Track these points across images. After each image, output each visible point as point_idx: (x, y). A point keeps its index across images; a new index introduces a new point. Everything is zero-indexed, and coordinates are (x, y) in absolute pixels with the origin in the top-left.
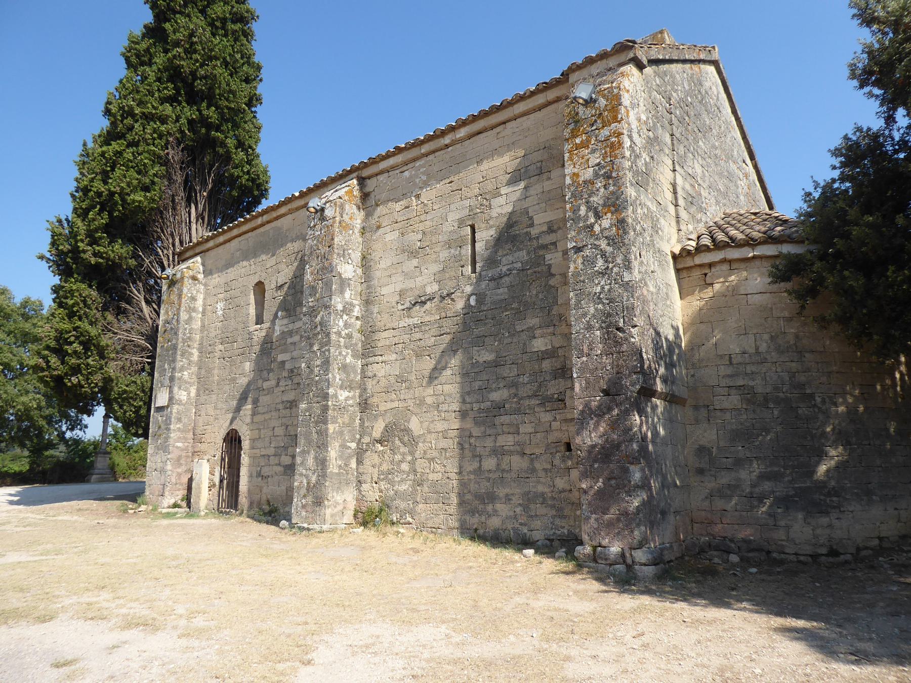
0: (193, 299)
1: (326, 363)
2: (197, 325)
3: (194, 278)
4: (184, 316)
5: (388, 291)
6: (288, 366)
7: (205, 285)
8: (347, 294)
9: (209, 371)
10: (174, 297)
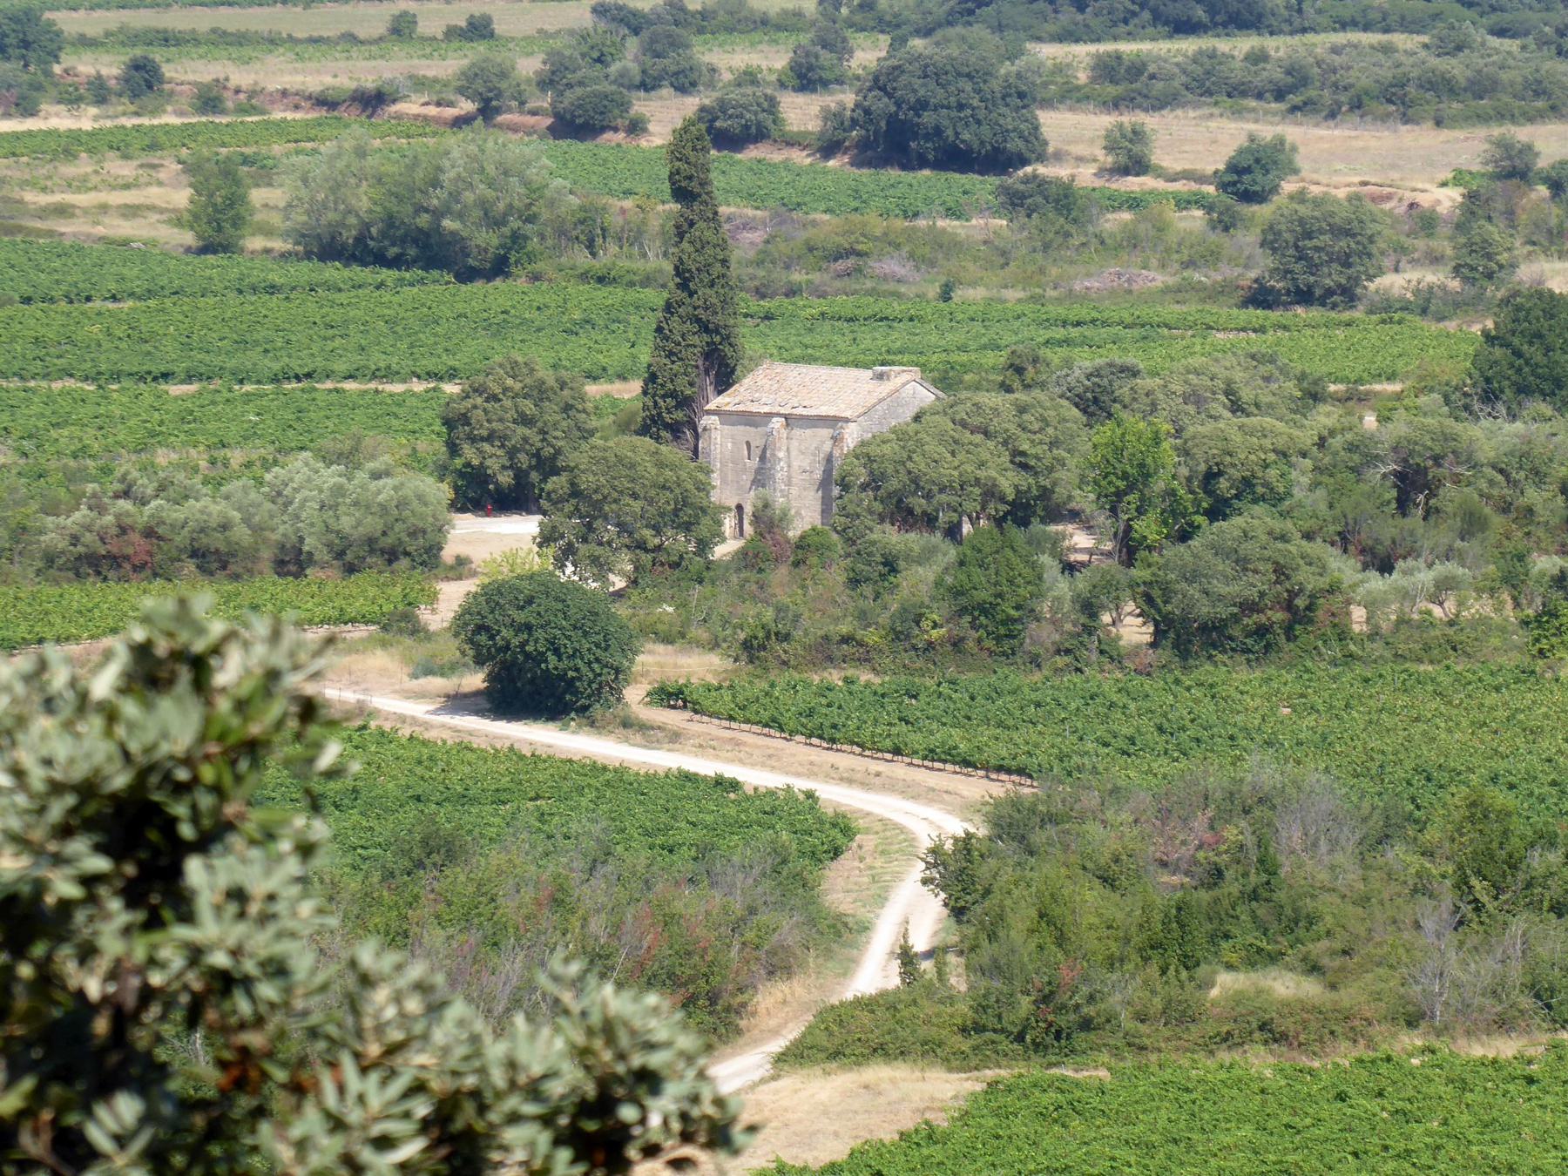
5: (795, 464)
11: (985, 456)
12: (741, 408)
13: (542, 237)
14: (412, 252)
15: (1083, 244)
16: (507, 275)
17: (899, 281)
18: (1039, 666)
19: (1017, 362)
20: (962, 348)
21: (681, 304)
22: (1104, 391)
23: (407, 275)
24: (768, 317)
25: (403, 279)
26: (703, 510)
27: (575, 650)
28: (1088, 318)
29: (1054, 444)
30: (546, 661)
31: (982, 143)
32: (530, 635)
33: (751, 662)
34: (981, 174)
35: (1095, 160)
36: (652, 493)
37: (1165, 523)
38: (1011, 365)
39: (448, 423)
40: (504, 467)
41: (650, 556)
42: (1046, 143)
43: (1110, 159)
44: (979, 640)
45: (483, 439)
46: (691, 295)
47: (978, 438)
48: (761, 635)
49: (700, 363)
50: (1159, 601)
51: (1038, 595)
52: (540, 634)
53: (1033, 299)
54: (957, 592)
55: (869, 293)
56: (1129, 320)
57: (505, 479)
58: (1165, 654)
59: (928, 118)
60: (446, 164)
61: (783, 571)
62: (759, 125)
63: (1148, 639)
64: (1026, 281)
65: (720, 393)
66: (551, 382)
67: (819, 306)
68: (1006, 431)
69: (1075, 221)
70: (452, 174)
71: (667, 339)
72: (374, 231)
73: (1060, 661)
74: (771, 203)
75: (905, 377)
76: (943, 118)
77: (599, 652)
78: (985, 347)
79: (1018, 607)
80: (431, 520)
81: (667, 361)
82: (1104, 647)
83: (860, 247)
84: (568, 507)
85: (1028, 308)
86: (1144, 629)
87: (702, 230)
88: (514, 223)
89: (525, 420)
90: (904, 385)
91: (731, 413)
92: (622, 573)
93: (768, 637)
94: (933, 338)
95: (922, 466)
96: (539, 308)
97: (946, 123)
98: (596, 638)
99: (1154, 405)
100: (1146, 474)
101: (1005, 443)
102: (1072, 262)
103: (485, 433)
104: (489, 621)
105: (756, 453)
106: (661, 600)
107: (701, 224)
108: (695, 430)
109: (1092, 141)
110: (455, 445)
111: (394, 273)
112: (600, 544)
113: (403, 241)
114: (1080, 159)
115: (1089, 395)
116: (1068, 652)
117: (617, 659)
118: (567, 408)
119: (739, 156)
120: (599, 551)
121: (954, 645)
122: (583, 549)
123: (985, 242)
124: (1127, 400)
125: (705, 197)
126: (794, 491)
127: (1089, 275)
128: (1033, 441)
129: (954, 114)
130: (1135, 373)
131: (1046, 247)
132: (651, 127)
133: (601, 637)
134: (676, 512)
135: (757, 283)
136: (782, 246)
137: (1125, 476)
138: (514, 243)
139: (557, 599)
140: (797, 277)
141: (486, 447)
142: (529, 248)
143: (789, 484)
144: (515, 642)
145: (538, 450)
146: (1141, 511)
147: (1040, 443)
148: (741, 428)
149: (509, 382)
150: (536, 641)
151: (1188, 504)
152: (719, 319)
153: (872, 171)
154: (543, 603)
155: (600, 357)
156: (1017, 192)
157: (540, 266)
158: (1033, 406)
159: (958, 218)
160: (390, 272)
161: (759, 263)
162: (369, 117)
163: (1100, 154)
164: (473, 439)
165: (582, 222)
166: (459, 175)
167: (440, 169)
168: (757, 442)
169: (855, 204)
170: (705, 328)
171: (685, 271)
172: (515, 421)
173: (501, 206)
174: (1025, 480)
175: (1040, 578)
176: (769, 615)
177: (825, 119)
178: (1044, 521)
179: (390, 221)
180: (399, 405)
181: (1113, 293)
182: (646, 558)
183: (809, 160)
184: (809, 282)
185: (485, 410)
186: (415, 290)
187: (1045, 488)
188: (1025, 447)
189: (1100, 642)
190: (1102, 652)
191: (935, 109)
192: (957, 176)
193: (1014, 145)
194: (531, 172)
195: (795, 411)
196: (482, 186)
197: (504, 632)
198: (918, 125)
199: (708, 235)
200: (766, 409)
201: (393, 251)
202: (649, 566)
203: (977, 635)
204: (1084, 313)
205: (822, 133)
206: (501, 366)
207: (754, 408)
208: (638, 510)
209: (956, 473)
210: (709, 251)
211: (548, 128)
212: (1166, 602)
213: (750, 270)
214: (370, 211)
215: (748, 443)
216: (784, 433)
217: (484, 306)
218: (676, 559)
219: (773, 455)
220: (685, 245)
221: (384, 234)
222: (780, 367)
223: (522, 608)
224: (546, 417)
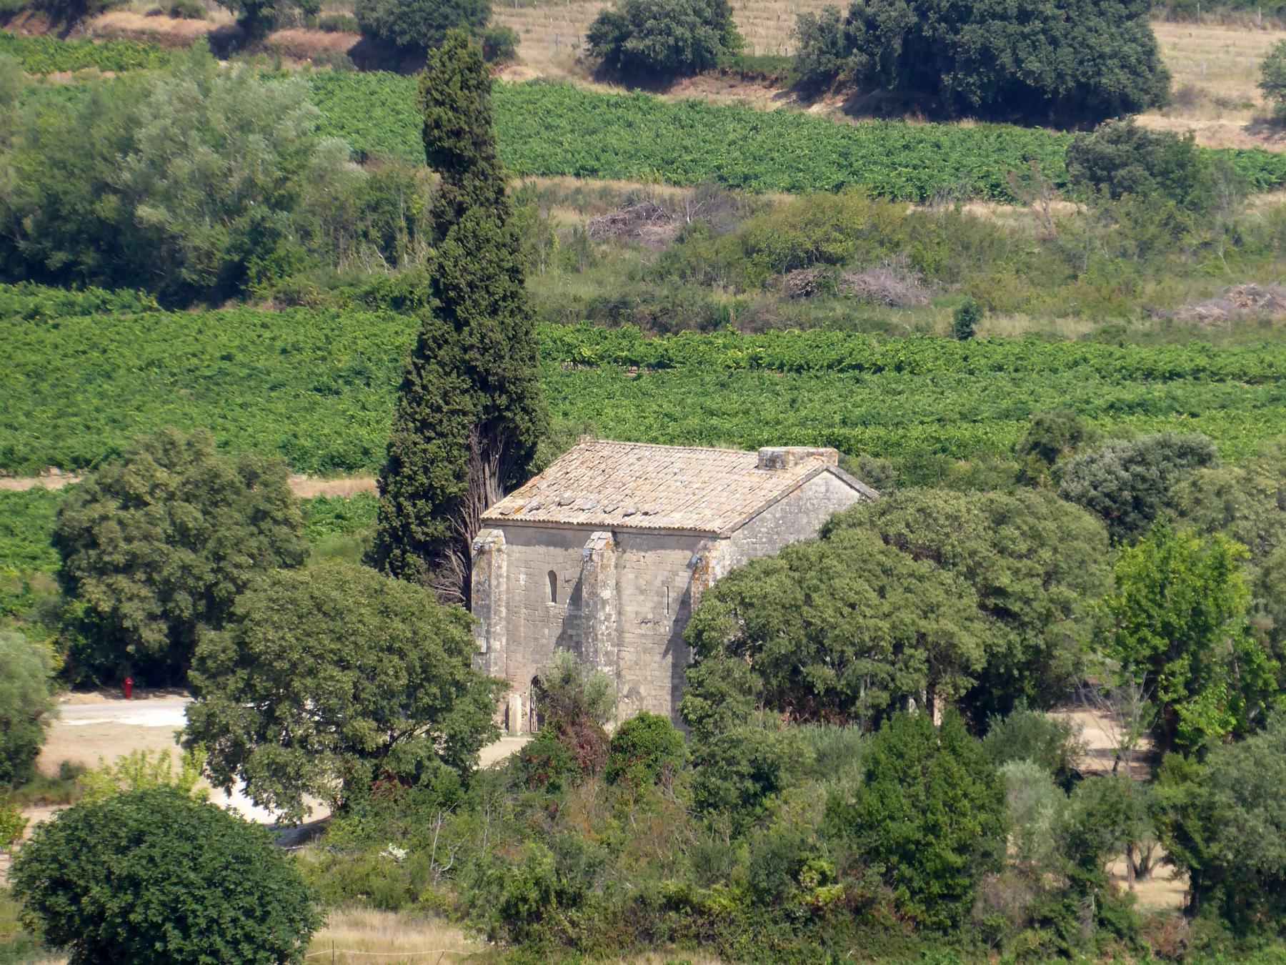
0: (499, 567)
1: (596, 652)
2: (503, 588)
3: (499, 550)
4: (494, 582)
5: (630, 609)
6: (575, 639)
7: (508, 555)
8: (607, 609)
9: (516, 627)
10: (483, 564)
11: (937, 595)
12: (541, 515)
13: (306, 234)
14: (90, 258)
15: (1206, 245)
16: (244, 296)
17: (892, 304)
18: (998, 946)
19: (1045, 439)
20: (968, 417)
21: (442, 342)
22: (1153, 486)
23: (79, 297)
24: (663, 364)
25: (72, 304)
26: (459, 686)
27: (212, 921)
28: (1188, 366)
29: (1050, 577)
30: (163, 938)
31: (1060, 76)
32: (137, 895)
33: (516, 940)
34: (1058, 127)
35: (1248, 106)
36: (371, 659)
37: (1233, 708)
38: (1036, 445)
39: (62, 542)
40: (152, 617)
41: (369, 764)
42: (1166, 77)
43: (1271, 104)
44: (898, 905)
45: (117, 570)
46: (459, 326)
47: (926, 566)
48: (534, 895)
49: (474, 440)
50: (1197, 838)
51: (996, 830)
52: (152, 894)
53: (1109, 335)
54: (865, 825)
55: (836, 324)
56: (1255, 370)
57: (155, 635)
58: (1210, 926)
59: (970, 34)
60: (144, 112)
61: (593, 787)
62: (697, 45)
63: (1178, 900)
64: (1098, 307)
65: (507, 490)
66: (231, 473)
67: (749, 344)
68: (973, 554)
69: (1195, 206)
70: (153, 129)
71: (419, 401)
72: (28, 223)
73: (1033, 938)
74: (700, 176)
75: (813, 464)
76: (998, 35)
77: (250, 924)
78: (1006, 415)
79: (961, 849)
80: (18, 703)
81: (417, 438)
82: (1107, 914)
83: (830, 248)
84: (234, 682)
85: (1094, 350)
86: (1177, 884)
87: (478, 219)
88: (257, 210)
89: (184, 537)
90: (809, 477)
91: (525, 524)
92: (321, 792)
93: (545, 899)
94: (923, 401)
95: (829, 613)
96: (284, 351)
97: (1001, 42)
98: (247, 901)
99: (1228, 509)
100: (1201, 626)
101: (971, 574)
102: (1185, 275)
103: (120, 559)
104: (72, 872)
105: (566, 591)
106: (385, 837)
107: (476, 210)
108: (466, 553)
109: (1248, 74)
110: (76, 580)
111: (60, 294)
112: (288, 744)
113: (73, 241)
114: (1222, 104)
115: (1127, 495)
116: (1046, 922)
117: (277, 934)
118: (258, 517)
119: (661, 98)
120: (284, 755)
121: (857, 911)
122: (259, 752)
123: (1044, 241)
124: (1185, 503)
125: (483, 164)
126: (628, 655)
127: (1205, 295)
128: (1016, 572)
129: (1013, 28)
130: (1203, 459)
131: (1145, 248)
132: (521, 51)
133: (253, 900)
134: (411, 690)
135: (656, 308)
136: (704, 249)
137: (1167, 630)
138: (256, 243)
139: (181, 835)
140: (721, 297)
141: (122, 581)
142: (281, 252)
143: (620, 643)
144: (113, 906)
145: (209, 588)
146: (1193, 688)
147: (1030, 575)
148: (541, 549)
149: (162, 475)
150: (147, 905)
151: (1270, 677)
152: (506, 367)
153: (877, 122)
154: (160, 842)
155: (363, 432)
156: (1102, 157)
157: (297, 281)
158: (1019, 513)
159: (1011, 200)
160: (52, 292)
161: (661, 275)
162: (62, 36)
163: (1256, 95)
164: (101, 570)
165: (375, 208)
166: (165, 129)
167: (134, 122)
168: (568, 573)
169: (840, 177)
170: (482, 382)
171: (447, 287)
172: (169, 540)
173: (235, 181)
174: (1003, 637)
175: (1000, 799)
176: (549, 861)
177: (806, 36)
178: (1032, 704)
179: (53, 206)
180: (15, 513)
181: (1239, 323)
182: (363, 768)
183: (779, 104)
184: (740, 307)
185: (120, 522)
186: (87, 320)
187: (1037, 650)
188: (1004, 580)
189: (1099, 905)
190: (1102, 923)
191: (982, 21)
192: (1018, 130)
193: (1114, 79)
194: (288, 128)
195: (629, 521)
196: (203, 149)
197: (95, 890)
198: (954, 45)
199: (488, 227)
200: (582, 518)
201: (58, 259)
202: (367, 780)
203: (893, 895)
204: (1185, 358)
205: (801, 60)
206: (148, 448)
207: (562, 516)
208: (348, 687)
209: (885, 625)
210: (489, 254)
211: (352, 53)
212: (1208, 841)
213: (642, 287)
214: (19, 192)
215: (553, 576)
216: (611, 557)
217: (197, 347)
218: (410, 768)
219: (594, 594)
220: (449, 244)
221: (43, 231)
222: (607, 448)
223: (122, 851)
224: (223, 532)
